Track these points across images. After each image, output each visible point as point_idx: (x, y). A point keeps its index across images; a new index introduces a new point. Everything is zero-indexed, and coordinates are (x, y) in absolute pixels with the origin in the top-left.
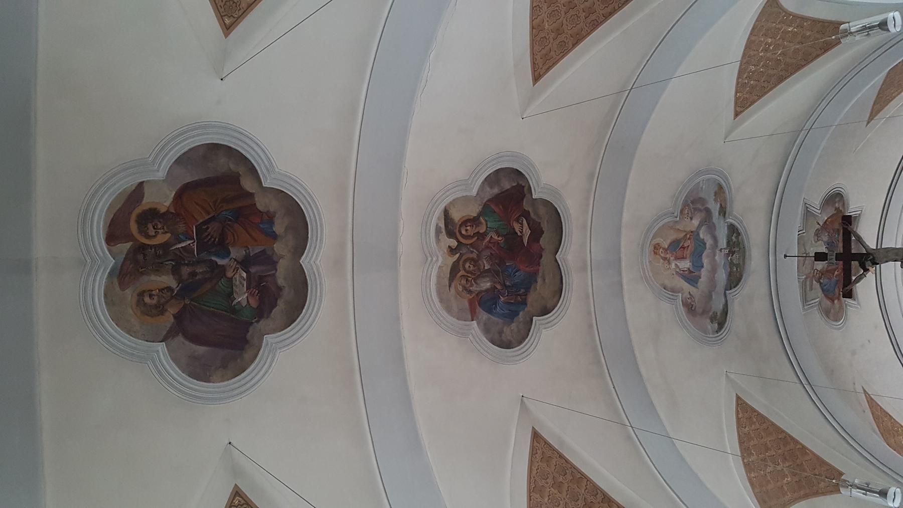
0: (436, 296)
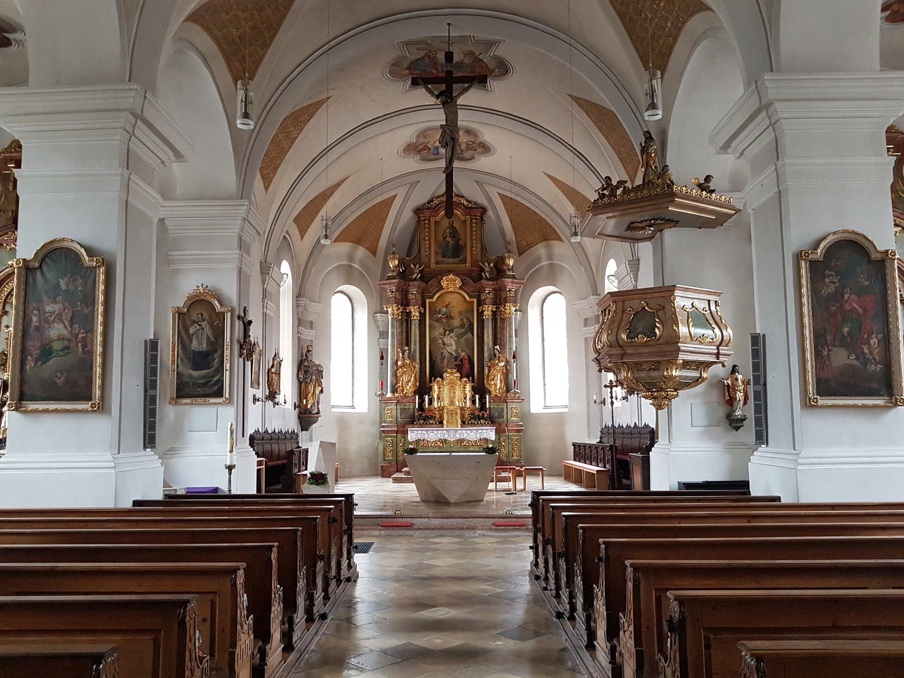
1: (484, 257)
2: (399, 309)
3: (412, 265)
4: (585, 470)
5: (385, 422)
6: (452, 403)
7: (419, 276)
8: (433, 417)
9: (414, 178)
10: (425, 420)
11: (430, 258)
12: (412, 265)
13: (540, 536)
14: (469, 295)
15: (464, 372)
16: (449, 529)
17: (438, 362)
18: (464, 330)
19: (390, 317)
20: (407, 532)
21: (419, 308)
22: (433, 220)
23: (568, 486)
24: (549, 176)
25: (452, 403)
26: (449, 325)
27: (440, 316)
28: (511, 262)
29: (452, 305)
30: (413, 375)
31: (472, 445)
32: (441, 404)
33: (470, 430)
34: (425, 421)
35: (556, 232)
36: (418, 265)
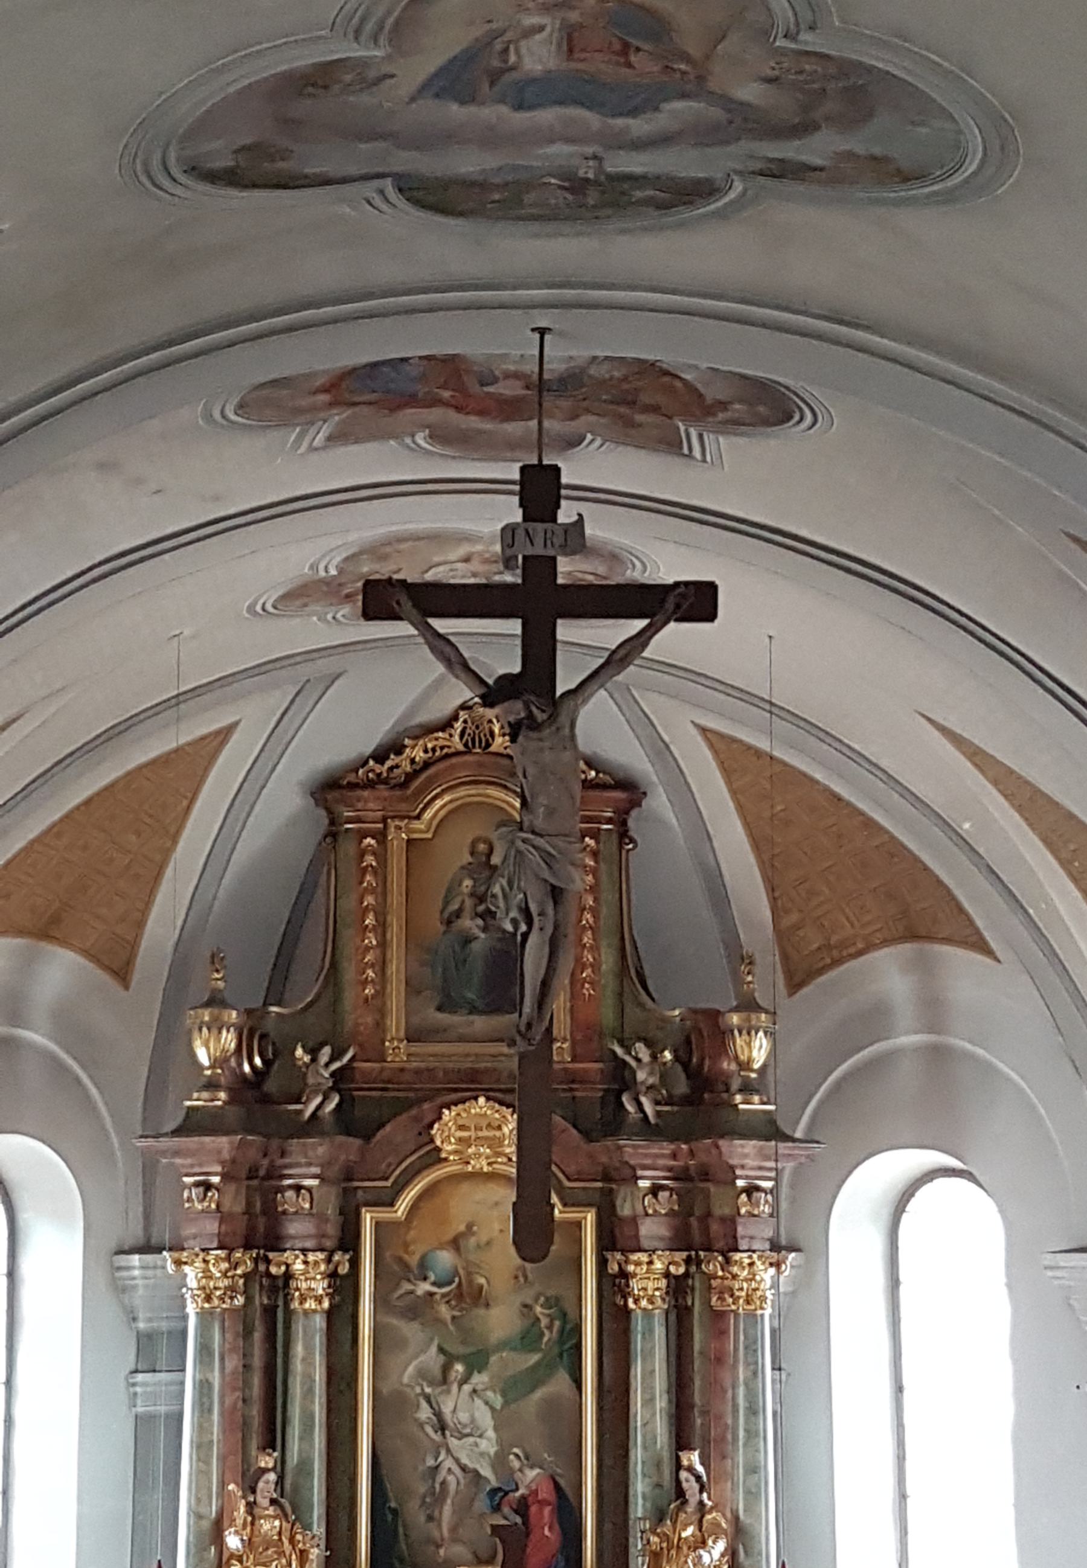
0: (665, 1386)
1: (630, 1009)
3: (299, 1052)
7: (331, 1106)
9: (325, 666)
12: (299, 1052)
17: (414, 1513)
18: (535, 1358)
22: (397, 838)
26: (466, 1334)
27: (424, 1287)
28: (759, 1050)
35: (961, 910)
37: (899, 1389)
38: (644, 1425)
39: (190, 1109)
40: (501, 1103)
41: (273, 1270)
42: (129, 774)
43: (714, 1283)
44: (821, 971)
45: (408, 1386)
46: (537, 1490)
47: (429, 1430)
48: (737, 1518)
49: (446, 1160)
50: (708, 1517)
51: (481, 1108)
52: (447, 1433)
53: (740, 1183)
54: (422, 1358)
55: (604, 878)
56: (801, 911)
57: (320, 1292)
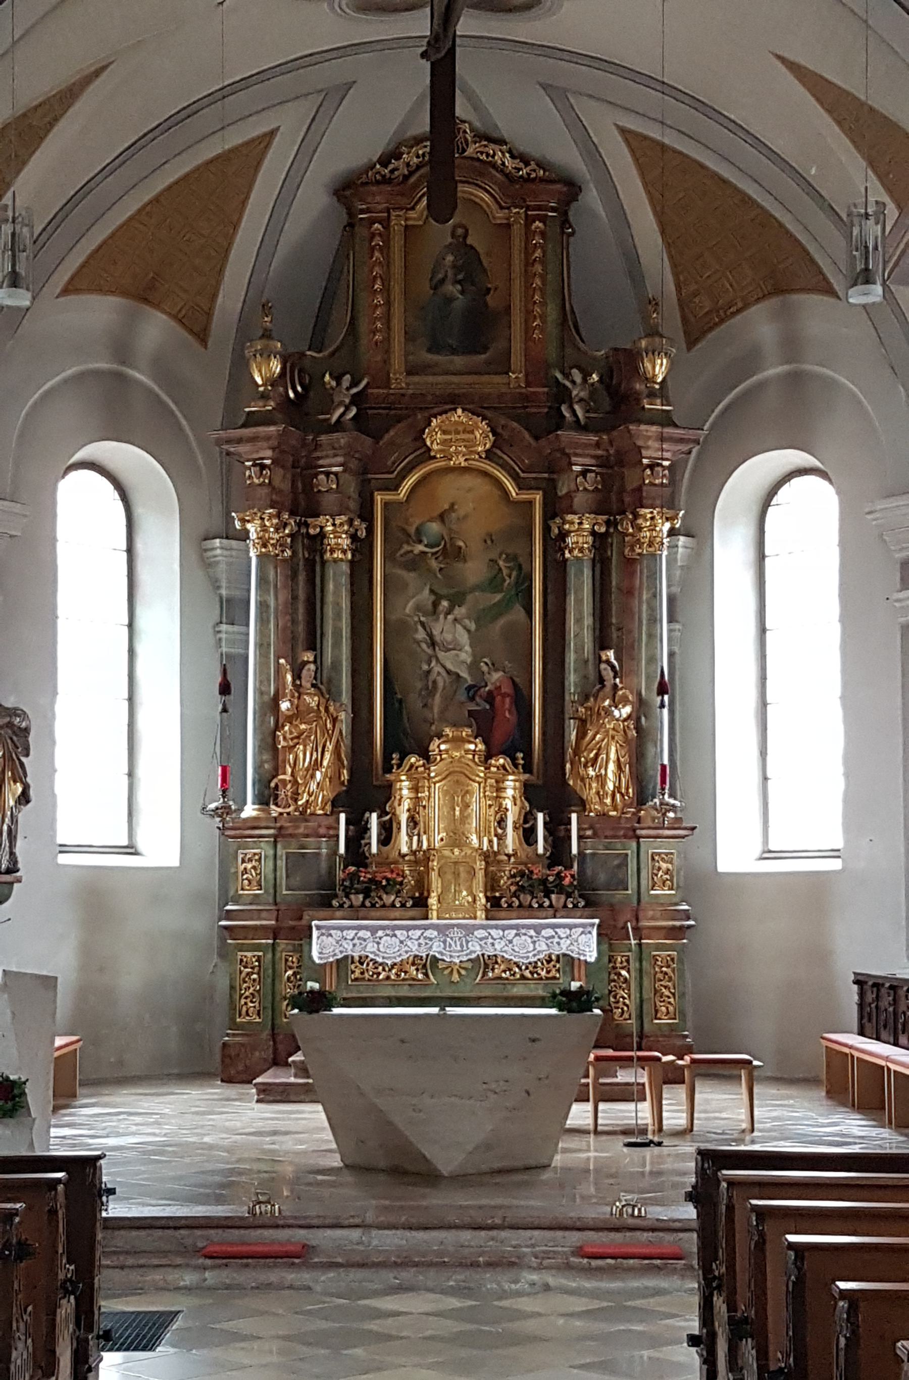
2: (285, 525)
4: (893, 1067)
5: (236, 902)
6: (456, 839)
8: (393, 886)
10: (367, 893)
11: (387, 352)
13: (719, 1303)
14: (515, 478)
15: (499, 735)
16: (431, 1265)
17: (414, 702)
18: (498, 597)
19: (253, 554)
20: (291, 1276)
21: (350, 522)
22: (397, 223)
23: (835, 1118)
24: (794, 67)
25: (456, 839)
27: (421, 548)
28: (659, 369)
29: (462, 513)
30: (330, 746)
31: (523, 977)
32: (420, 841)
33: (516, 927)
34: (367, 896)
35: (812, 261)
36: (348, 377)
37: (762, 630)
38: (575, 636)
39: (249, 413)
40: (473, 414)
41: (312, 531)
42: (197, 169)
43: (627, 539)
44: (711, 329)
45: (408, 616)
46: (500, 687)
47: (424, 646)
48: (639, 694)
49: (434, 457)
50: (620, 693)
51: (459, 417)
52: (437, 648)
53: (645, 461)
54: (418, 597)
55: (549, 251)
56: (696, 283)
57: (345, 547)
